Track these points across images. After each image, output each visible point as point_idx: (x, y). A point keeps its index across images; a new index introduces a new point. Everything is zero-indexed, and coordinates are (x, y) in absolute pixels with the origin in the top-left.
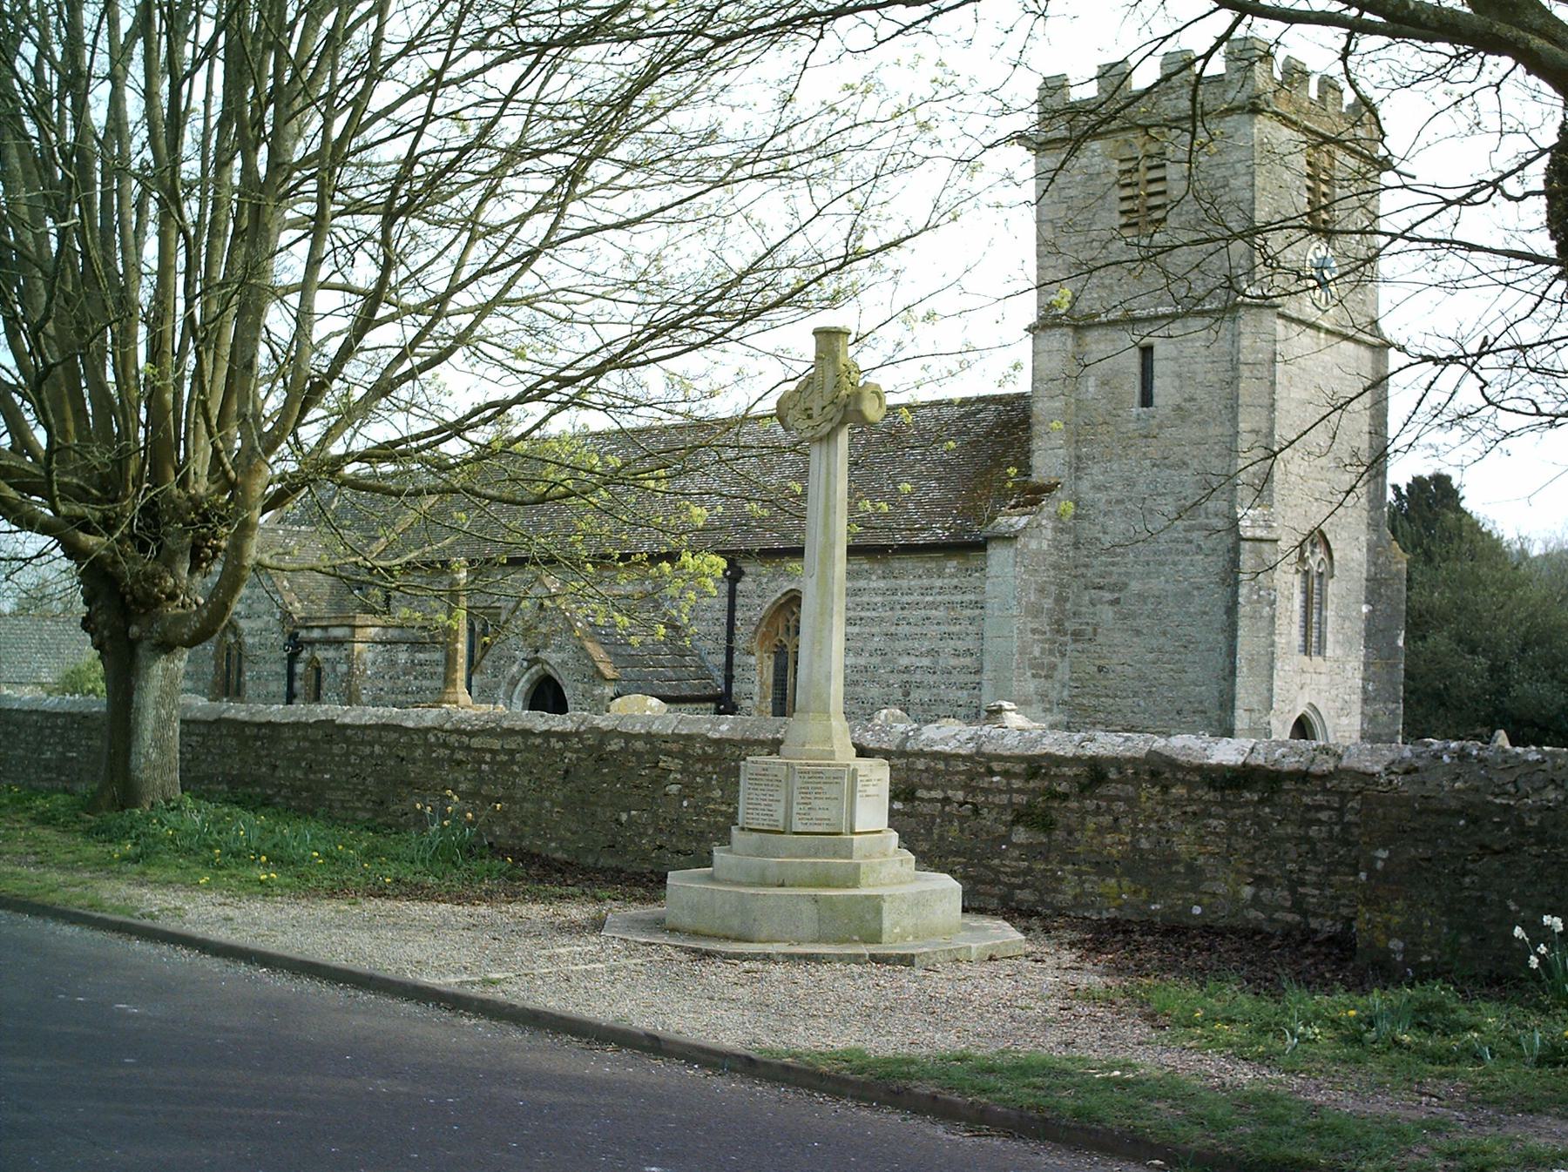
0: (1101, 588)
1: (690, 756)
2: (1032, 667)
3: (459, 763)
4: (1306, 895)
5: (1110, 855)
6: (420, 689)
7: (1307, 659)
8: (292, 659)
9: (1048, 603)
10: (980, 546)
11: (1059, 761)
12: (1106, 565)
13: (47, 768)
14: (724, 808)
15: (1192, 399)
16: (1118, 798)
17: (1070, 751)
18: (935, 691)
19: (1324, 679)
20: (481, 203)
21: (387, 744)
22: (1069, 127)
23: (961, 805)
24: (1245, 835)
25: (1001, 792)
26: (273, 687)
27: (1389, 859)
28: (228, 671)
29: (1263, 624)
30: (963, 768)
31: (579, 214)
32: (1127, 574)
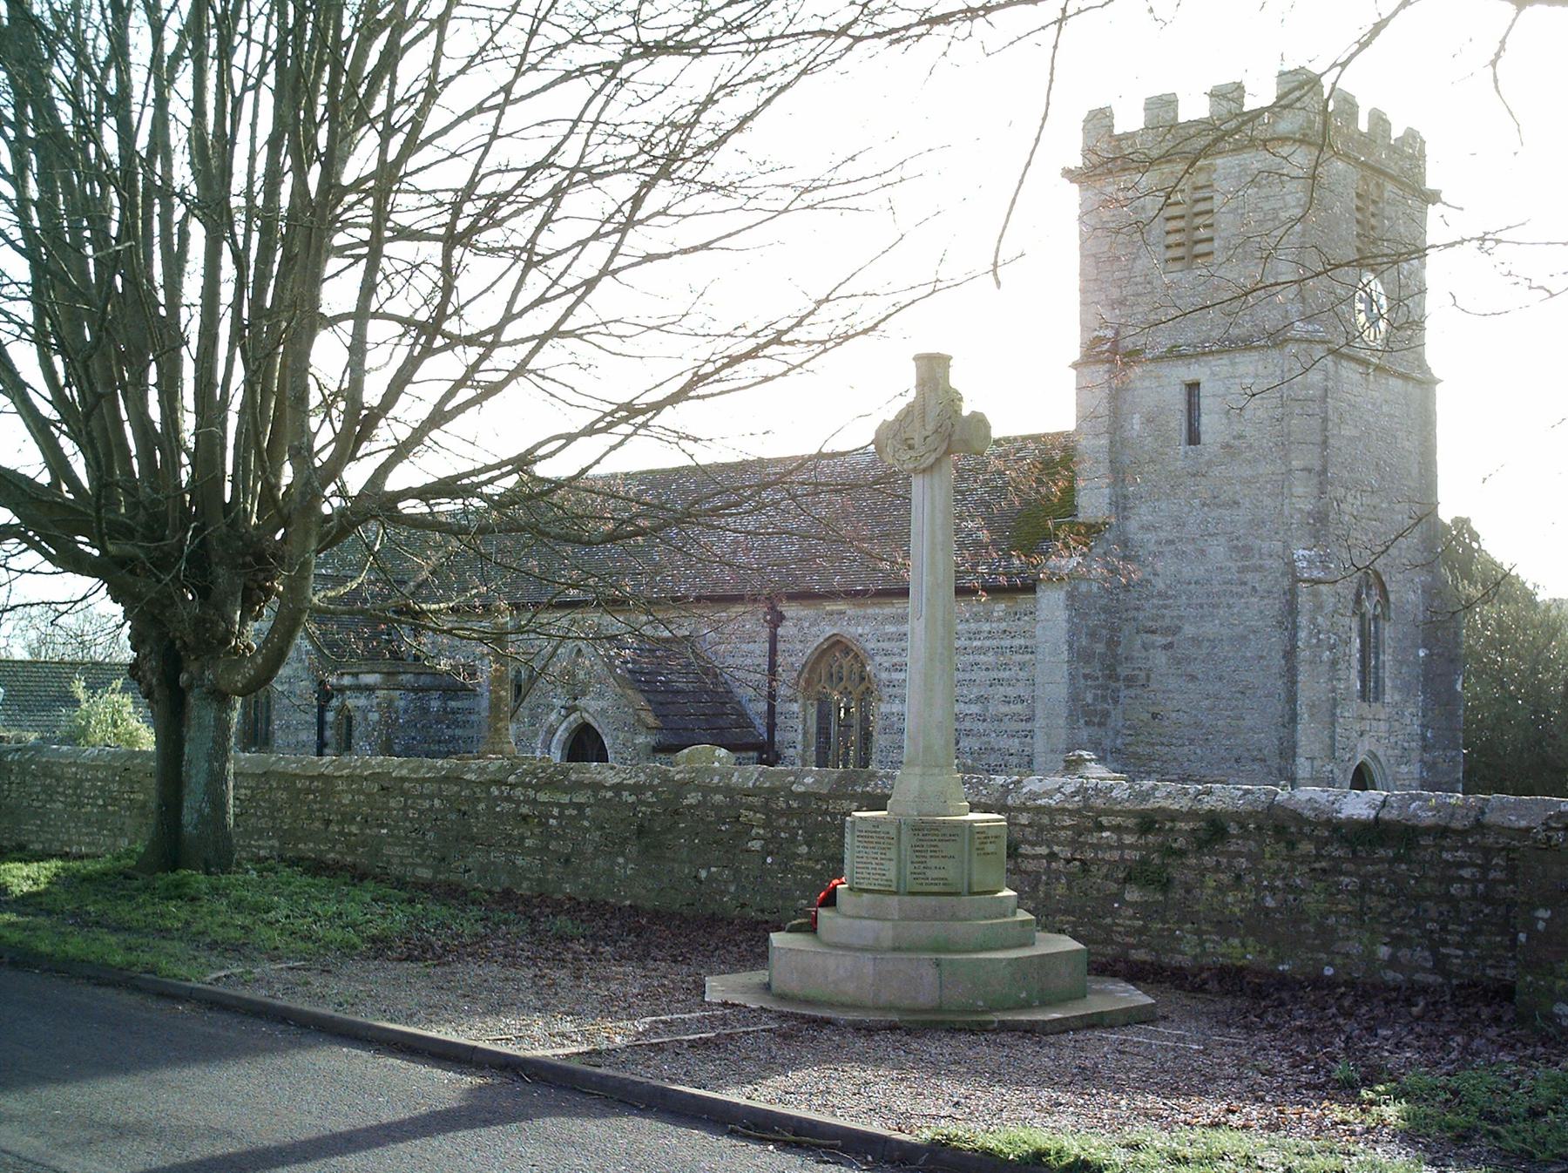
0: (1153, 632)
1: (772, 810)
2: (1085, 714)
3: (525, 818)
4: (1449, 956)
5: (1233, 913)
6: (453, 738)
7: (1365, 705)
8: (322, 710)
9: (1100, 648)
10: (1030, 588)
11: (1174, 816)
12: (1159, 608)
13: (88, 823)
14: (811, 864)
15: (1240, 437)
16: (1239, 854)
17: (1183, 804)
18: (985, 739)
19: (1383, 726)
20: (539, 229)
21: (448, 798)
22: (1108, 160)
23: (1068, 861)
24: (1381, 894)
25: (1111, 847)
26: (303, 736)
27: (1551, 918)
28: (256, 720)
29: (1324, 668)
30: (1068, 822)
31: (637, 242)
32: (1180, 618)
